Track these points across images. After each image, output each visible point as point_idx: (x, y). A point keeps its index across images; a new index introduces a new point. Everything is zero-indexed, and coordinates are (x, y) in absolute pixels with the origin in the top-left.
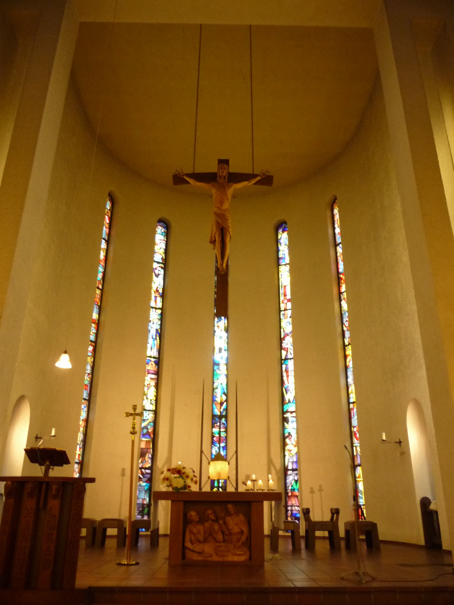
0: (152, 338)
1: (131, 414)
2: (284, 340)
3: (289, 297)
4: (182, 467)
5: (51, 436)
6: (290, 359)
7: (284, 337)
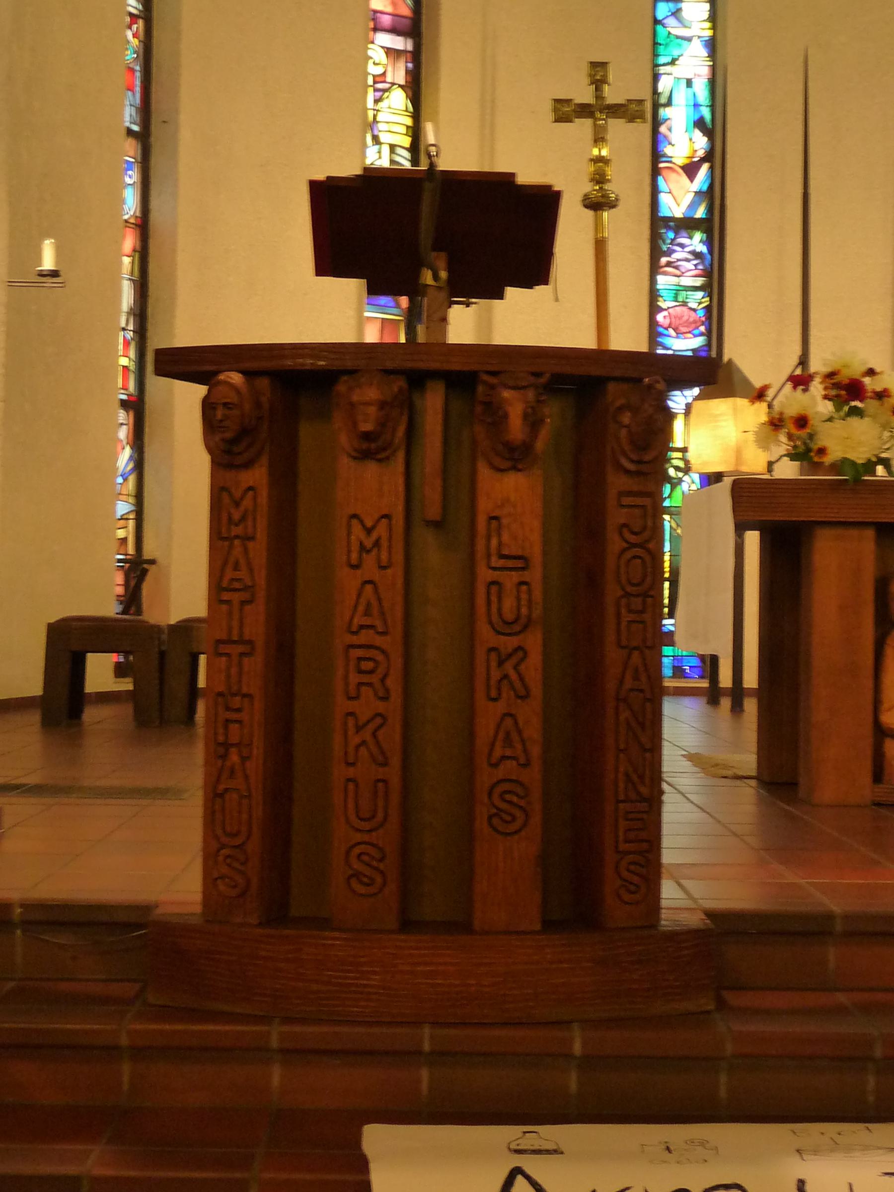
1: (585, 111)
4: (864, 368)
5: (42, 274)
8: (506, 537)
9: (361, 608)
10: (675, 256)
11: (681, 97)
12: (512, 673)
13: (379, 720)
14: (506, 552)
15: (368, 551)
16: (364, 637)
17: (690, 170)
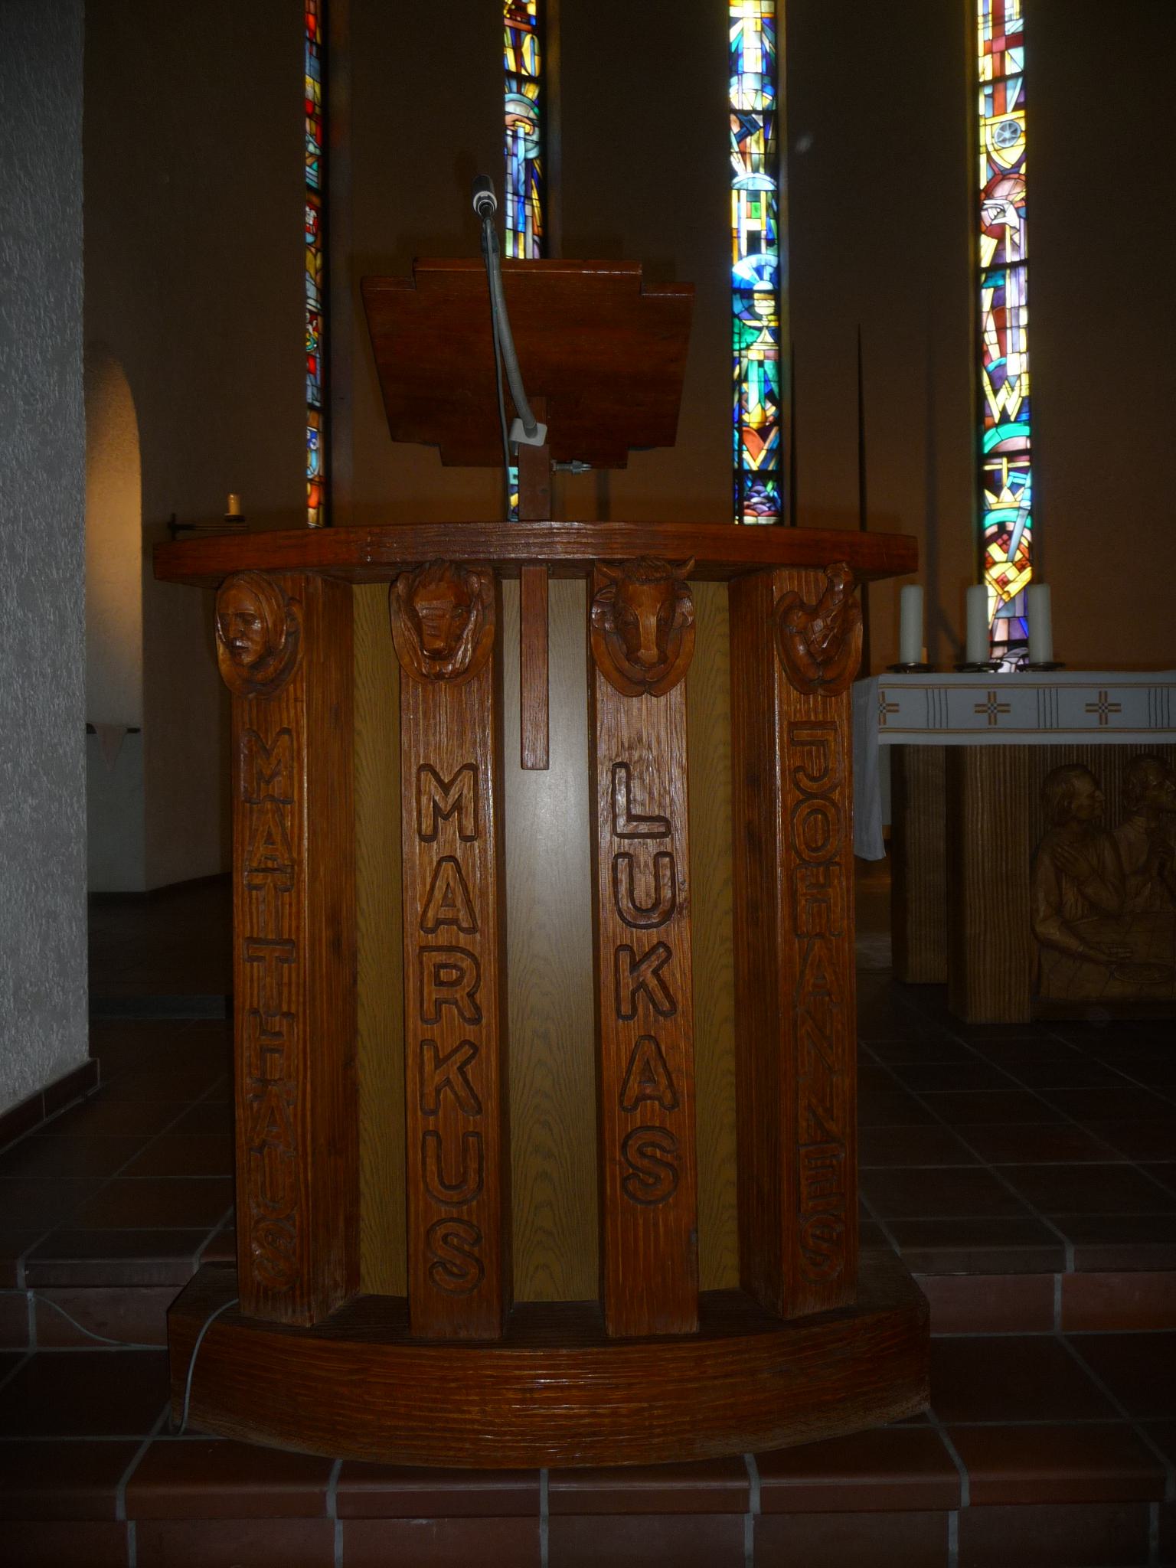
0: (516, 193)
2: (989, 196)
3: (1014, 25)
6: (1014, 266)
7: (993, 184)
8: (638, 793)
9: (438, 895)
10: (754, 500)
11: (754, 374)
12: (653, 982)
13: (467, 1051)
14: (637, 810)
15: (446, 817)
16: (443, 937)
17: (763, 432)
